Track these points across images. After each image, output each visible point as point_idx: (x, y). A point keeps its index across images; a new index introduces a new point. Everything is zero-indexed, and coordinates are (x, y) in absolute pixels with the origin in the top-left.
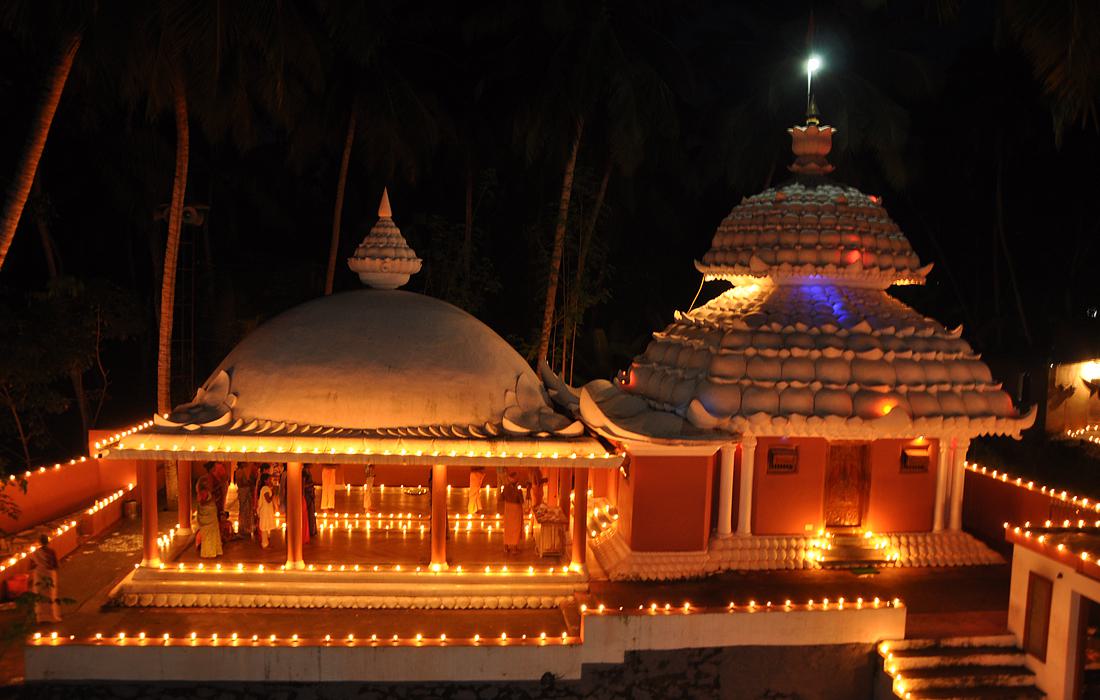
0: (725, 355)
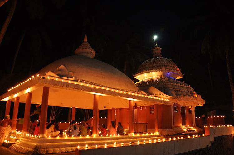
0: (168, 84)
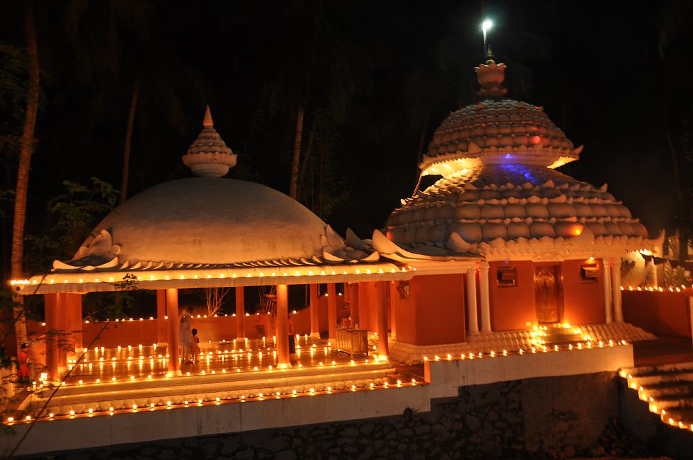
0: (465, 205)
